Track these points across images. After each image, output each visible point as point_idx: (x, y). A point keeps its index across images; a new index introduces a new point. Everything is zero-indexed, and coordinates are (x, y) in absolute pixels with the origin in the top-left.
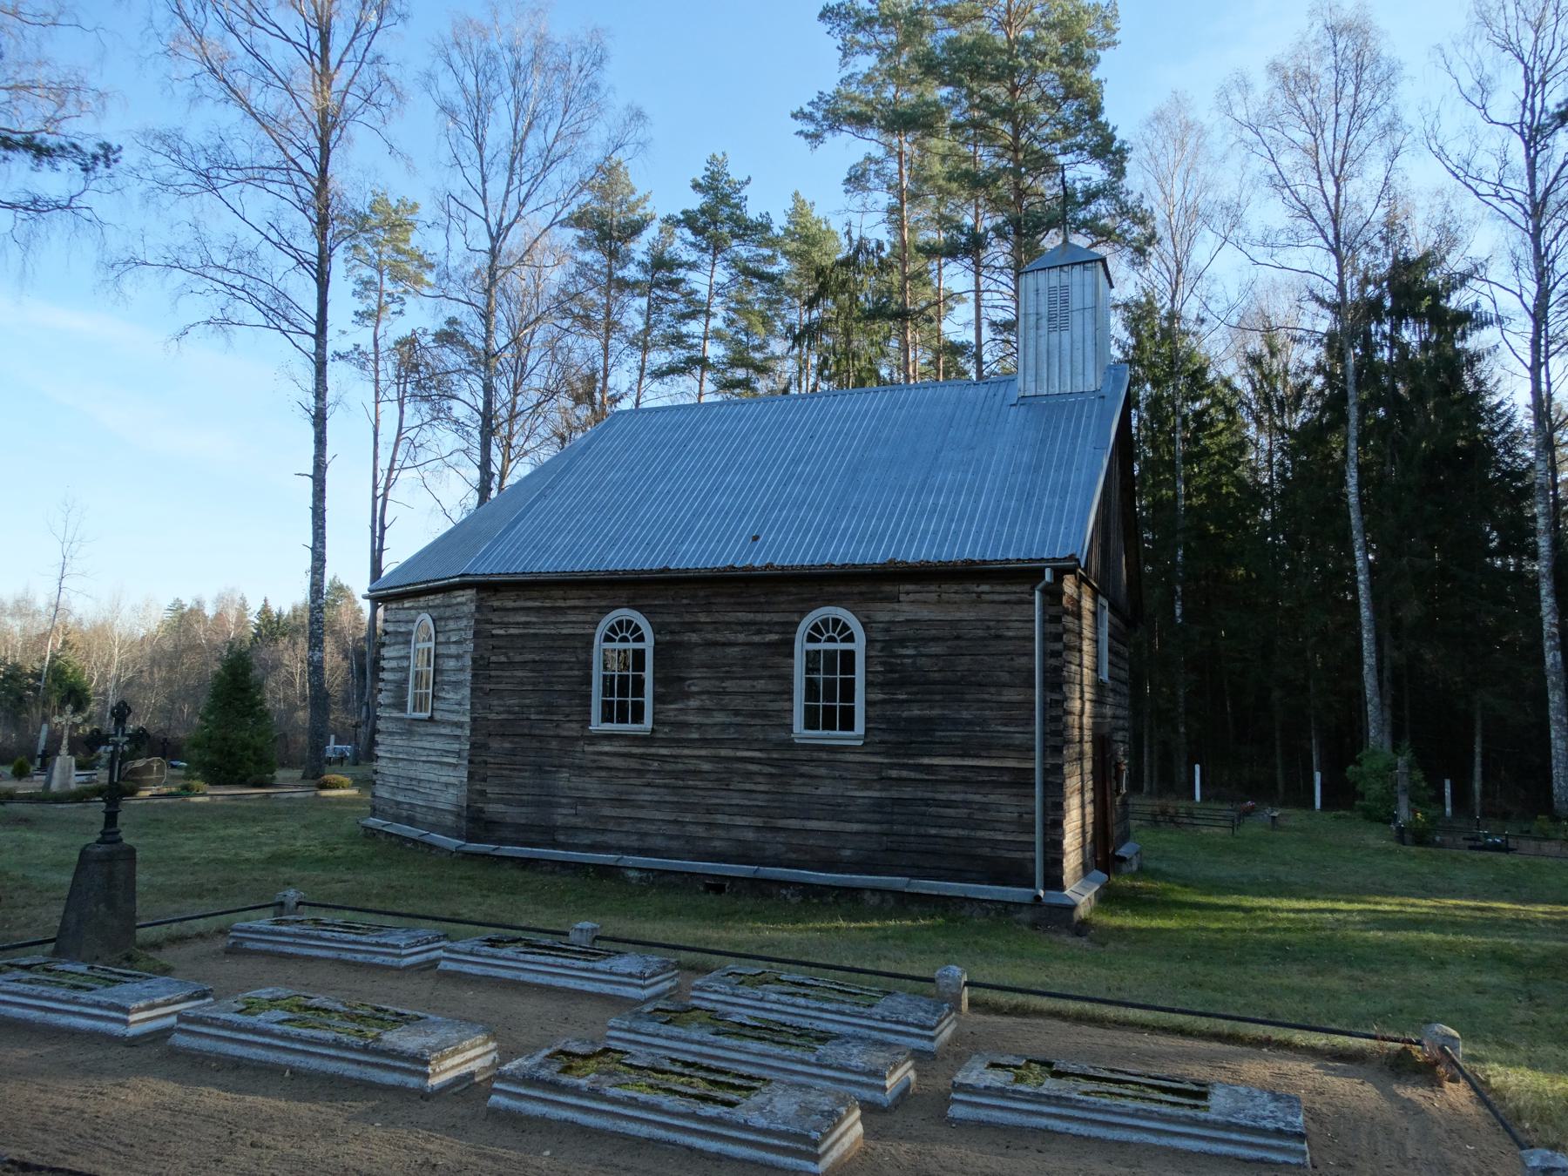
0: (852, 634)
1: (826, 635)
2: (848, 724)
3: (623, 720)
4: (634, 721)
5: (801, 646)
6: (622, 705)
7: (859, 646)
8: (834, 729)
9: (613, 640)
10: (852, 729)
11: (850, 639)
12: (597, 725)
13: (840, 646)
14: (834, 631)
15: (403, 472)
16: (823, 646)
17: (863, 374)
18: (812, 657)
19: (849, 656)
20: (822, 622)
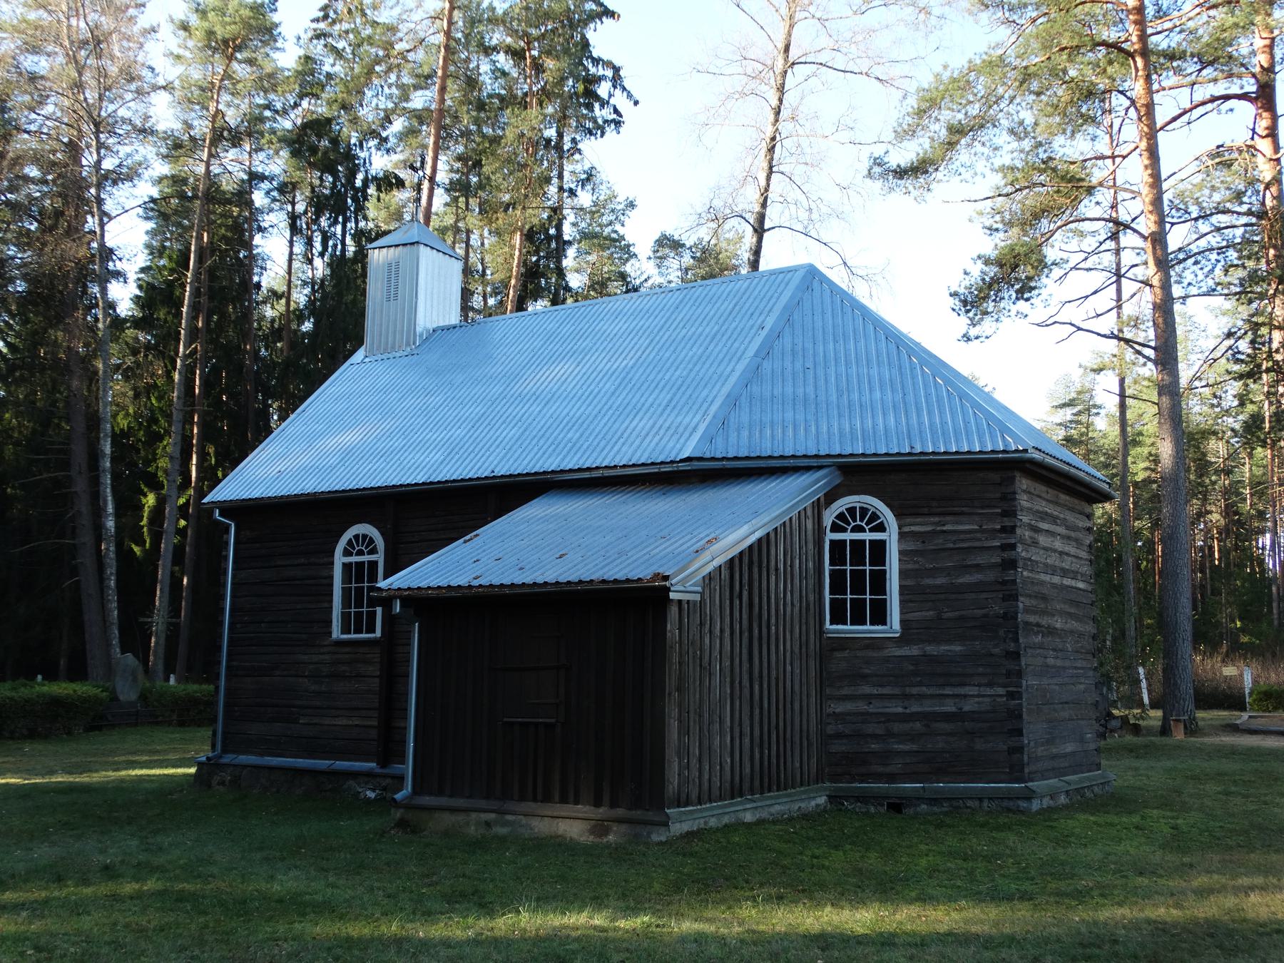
0: (371, 538)
1: (850, 528)
2: (880, 616)
3: (358, 631)
4: (367, 632)
5: (339, 559)
6: (359, 615)
7: (892, 537)
8: (864, 623)
9: (351, 554)
10: (374, 631)
11: (881, 528)
12: (336, 633)
13: (868, 536)
14: (855, 520)
15: (1074, 272)
16: (848, 536)
17: (226, 134)
18: (346, 567)
19: (879, 549)
20: (861, 508)
